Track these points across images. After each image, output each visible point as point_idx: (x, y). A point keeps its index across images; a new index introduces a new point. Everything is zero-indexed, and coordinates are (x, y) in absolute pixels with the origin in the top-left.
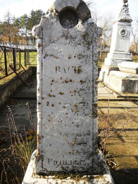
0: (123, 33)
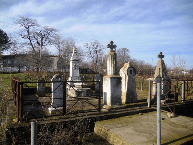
0: (75, 66)
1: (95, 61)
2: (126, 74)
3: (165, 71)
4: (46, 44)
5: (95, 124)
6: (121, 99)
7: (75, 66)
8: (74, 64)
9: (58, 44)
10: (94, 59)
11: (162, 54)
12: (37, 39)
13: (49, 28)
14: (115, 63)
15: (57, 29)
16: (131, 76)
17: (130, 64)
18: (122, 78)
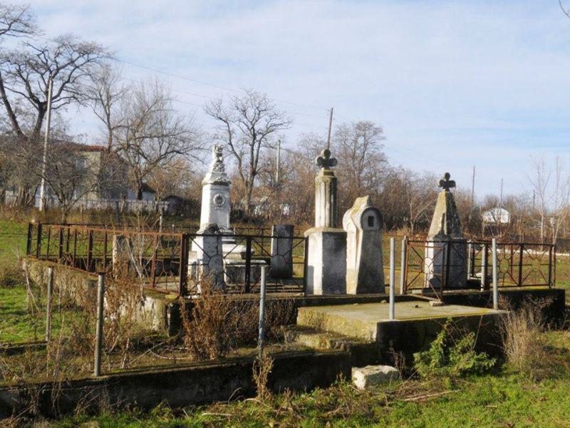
1: (249, 170)
2: (359, 226)
3: (455, 220)
4: (62, 102)
5: (297, 311)
6: (346, 282)
7: (219, 198)
8: (216, 193)
9: (105, 103)
10: (243, 163)
11: (450, 179)
12: (27, 82)
13: (76, 42)
14: (332, 201)
15: (107, 48)
16: (371, 230)
17: (369, 202)
18: (348, 235)
